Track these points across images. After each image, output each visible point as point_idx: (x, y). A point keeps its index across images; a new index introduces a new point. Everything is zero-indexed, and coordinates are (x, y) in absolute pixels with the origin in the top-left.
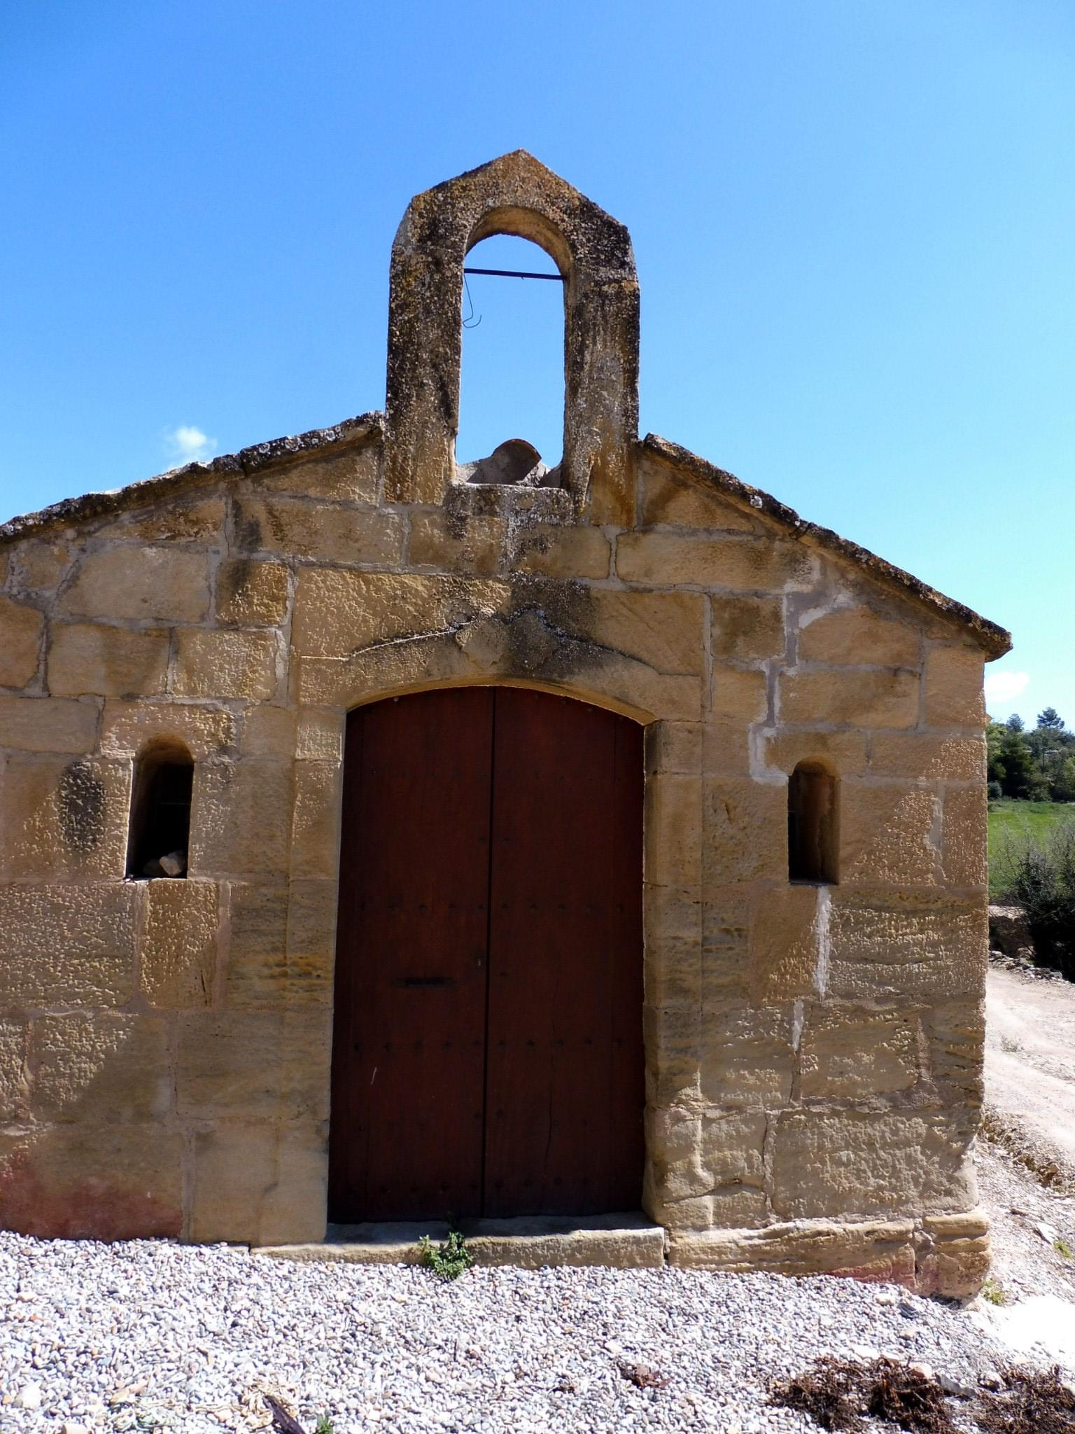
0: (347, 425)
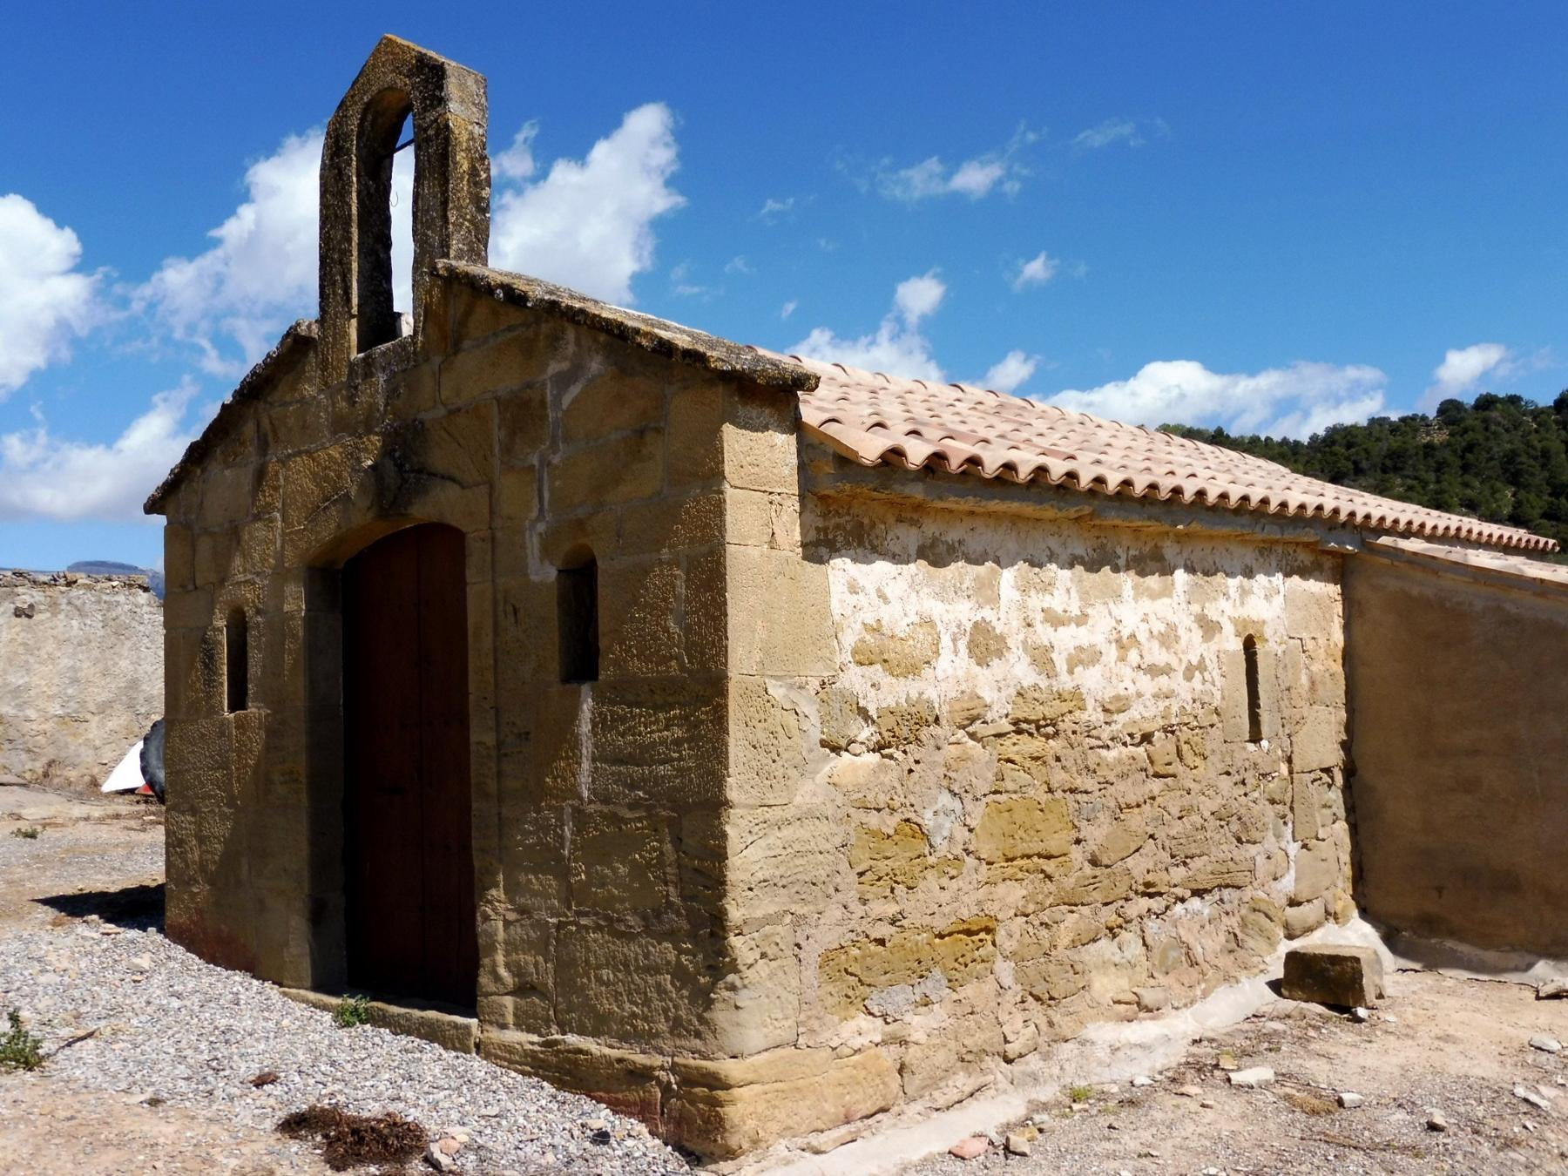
0: (282, 343)
